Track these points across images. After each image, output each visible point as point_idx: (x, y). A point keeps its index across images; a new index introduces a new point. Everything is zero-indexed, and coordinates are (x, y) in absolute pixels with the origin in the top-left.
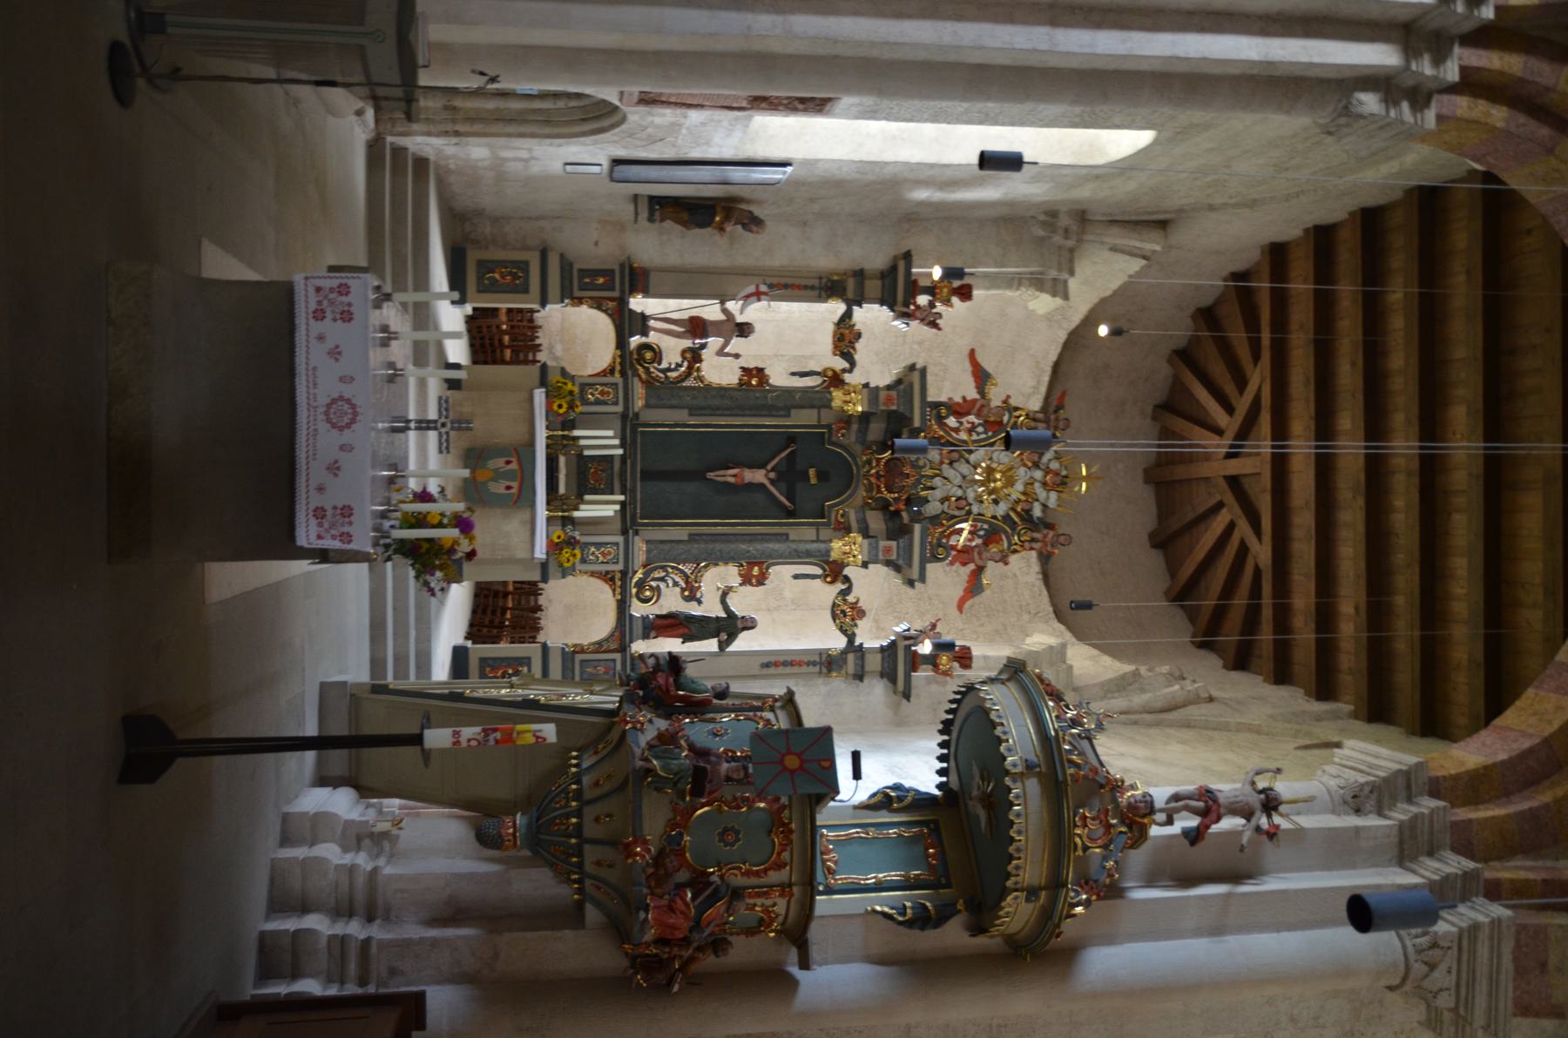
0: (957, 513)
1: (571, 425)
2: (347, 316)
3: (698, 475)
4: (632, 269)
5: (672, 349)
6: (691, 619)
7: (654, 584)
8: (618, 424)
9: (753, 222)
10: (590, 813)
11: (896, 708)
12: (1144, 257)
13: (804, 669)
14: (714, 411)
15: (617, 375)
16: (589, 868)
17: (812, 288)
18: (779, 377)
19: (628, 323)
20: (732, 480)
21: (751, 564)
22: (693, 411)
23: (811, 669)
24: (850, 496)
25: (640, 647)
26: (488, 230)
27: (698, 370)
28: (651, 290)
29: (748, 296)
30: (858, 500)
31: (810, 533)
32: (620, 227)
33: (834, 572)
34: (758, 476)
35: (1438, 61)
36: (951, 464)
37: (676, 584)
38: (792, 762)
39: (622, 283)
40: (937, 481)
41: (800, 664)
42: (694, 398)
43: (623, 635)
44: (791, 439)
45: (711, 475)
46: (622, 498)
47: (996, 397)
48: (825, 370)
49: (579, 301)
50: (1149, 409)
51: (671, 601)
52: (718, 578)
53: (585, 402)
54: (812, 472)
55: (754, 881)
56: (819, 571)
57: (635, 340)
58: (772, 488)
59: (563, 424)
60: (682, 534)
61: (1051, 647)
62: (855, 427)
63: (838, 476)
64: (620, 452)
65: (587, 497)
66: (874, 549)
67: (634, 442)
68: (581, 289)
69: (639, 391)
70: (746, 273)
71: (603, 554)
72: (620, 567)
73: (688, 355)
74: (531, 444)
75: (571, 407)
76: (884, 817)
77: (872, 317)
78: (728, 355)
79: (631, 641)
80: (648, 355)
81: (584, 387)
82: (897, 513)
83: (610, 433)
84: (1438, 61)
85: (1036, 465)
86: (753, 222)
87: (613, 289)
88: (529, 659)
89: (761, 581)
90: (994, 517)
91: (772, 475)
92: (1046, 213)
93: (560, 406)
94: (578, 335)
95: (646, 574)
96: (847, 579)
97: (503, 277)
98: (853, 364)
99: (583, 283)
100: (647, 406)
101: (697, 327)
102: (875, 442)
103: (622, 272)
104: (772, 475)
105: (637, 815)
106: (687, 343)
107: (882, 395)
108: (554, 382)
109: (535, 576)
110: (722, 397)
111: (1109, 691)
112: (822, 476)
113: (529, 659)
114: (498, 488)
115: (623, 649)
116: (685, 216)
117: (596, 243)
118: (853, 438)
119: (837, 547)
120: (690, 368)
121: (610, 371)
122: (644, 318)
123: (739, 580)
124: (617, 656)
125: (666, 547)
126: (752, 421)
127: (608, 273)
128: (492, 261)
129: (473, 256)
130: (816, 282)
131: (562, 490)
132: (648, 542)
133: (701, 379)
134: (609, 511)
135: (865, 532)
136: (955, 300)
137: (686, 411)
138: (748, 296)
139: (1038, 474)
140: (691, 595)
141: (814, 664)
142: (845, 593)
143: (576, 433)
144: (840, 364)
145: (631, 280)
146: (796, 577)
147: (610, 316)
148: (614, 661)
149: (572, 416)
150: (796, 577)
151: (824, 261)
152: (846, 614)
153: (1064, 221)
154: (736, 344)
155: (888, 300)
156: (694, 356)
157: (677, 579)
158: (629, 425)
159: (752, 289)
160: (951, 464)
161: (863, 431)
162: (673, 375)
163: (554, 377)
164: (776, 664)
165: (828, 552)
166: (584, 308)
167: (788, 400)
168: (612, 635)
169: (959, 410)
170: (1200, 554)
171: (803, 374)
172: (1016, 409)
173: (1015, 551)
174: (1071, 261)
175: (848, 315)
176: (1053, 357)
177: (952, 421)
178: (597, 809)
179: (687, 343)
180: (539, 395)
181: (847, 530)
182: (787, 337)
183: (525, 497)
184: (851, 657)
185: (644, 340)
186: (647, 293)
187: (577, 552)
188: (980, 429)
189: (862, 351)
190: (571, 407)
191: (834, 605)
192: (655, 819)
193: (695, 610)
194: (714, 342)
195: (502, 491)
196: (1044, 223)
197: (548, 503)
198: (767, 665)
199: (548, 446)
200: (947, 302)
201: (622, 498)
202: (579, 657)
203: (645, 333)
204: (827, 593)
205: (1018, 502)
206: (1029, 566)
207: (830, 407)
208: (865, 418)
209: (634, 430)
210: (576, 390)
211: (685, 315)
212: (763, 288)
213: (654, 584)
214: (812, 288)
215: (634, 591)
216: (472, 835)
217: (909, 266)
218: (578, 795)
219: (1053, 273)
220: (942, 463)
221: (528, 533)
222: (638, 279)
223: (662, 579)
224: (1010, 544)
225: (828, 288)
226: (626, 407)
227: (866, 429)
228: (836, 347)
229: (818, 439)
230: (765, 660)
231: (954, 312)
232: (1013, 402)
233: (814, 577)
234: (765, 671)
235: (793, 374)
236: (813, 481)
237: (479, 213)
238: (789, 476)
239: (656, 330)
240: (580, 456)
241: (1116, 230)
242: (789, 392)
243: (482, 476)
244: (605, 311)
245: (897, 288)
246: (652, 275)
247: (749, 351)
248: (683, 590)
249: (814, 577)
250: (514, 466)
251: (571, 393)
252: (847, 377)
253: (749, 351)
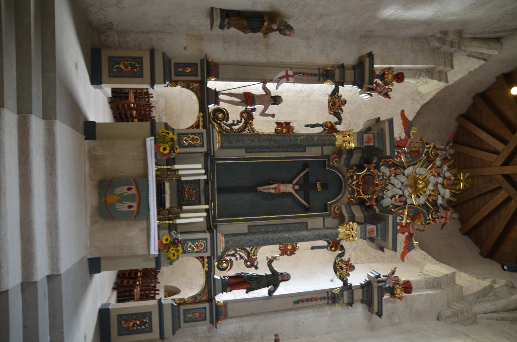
0: (399, 204)
1: (171, 161)
3: (252, 189)
4: (208, 61)
5: (235, 113)
6: (252, 278)
7: (228, 258)
8: (202, 159)
9: (286, 29)
11: (370, 320)
12: (485, 60)
13: (319, 302)
14: (261, 149)
15: (201, 127)
17: (315, 75)
18: (299, 129)
19: (206, 97)
20: (273, 191)
22: (248, 150)
23: (323, 302)
25: (221, 298)
26: (116, 40)
27: (251, 124)
28: (220, 77)
29: (281, 78)
30: (345, 199)
32: (200, 38)
33: (334, 244)
34: (288, 188)
36: (396, 175)
39: (202, 71)
41: (316, 299)
42: (252, 141)
43: (210, 291)
44: (306, 165)
45: (260, 189)
46: (207, 207)
48: (326, 123)
49: (175, 83)
51: (238, 268)
53: (182, 146)
54: (318, 184)
56: (325, 243)
57: (211, 107)
59: (167, 161)
61: (447, 275)
62: (344, 156)
64: (205, 177)
65: (185, 208)
67: (213, 170)
69: (217, 138)
70: (278, 66)
71: (197, 246)
74: (146, 176)
75: (172, 149)
77: (348, 91)
78: (268, 115)
79: (215, 295)
80: (220, 115)
81: (181, 135)
82: (370, 207)
83: (200, 166)
85: (439, 175)
86: (286, 29)
87: (197, 75)
88: (150, 313)
89: (292, 252)
91: (297, 187)
92: (442, 32)
93: (165, 149)
94: (176, 103)
96: (342, 248)
98: (340, 119)
99: (177, 72)
100: (222, 147)
101: (248, 99)
102: (354, 165)
103: (202, 65)
104: (297, 187)
106: (243, 108)
108: (162, 134)
109: (152, 265)
110: (270, 140)
111: (478, 297)
112: (324, 186)
113: (150, 313)
114: (123, 207)
115: (211, 300)
116: (245, 23)
117: (185, 48)
118: (342, 163)
120: (246, 123)
121: (197, 126)
122: (216, 93)
124: (207, 305)
125: (238, 238)
126: (283, 155)
127: (194, 65)
130: (317, 72)
131: (168, 205)
132: (225, 235)
133: (253, 130)
134: (199, 218)
137: (244, 150)
138: (281, 78)
139: (440, 180)
140: (251, 262)
141: (324, 298)
143: (176, 167)
145: (208, 69)
146: (313, 248)
147: (195, 92)
148: (205, 308)
149: (173, 155)
151: (321, 60)
152: (342, 268)
153: (452, 37)
154: (272, 109)
155: (359, 82)
156: (248, 116)
157: (242, 254)
158: (209, 160)
159: (283, 73)
160: (395, 176)
161: (348, 159)
163: (160, 130)
164: (302, 301)
166: (179, 87)
167: (309, 140)
168: (203, 291)
170: (485, 211)
174: (452, 61)
179: (243, 108)
180: (150, 142)
182: (302, 104)
183: (142, 213)
184: (345, 293)
185: (216, 106)
186: (218, 78)
187: (180, 248)
190: (172, 149)
191: (335, 263)
193: (252, 271)
195: (126, 209)
196: (439, 39)
197: (159, 214)
198: (297, 302)
199: (157, 176)
201: (207, 207)
202: (182, 308)
203: (217, 102)
204: (330, 256)
205: (430, 195)
207: (334, 145)
209: (212, 162)
210: (175, 137)
211: (241, 91)
212: (290, 73)
213: (228, 258)
214: (315, 75)
215: (216, 263)
217: (372, 64)
219: (441, 68)
220: (390, 175)
221: (145, 237)
222: (212, 70)
223: (233, 255)
224: (426, 220)
225: (323, 75)
226: (209, 148)
227: (351, 157)
228: (330, 109)
229: (322, 163)
230: (296, 299)
234: (297, 306)
235: (307, 126)
236: (319, 189)
237: (109, 26)
238: (306, 187)
239: (223, 101)
240: (179, 181)
241: (475, 43)
243: (111, 199)
244: (192, 90)
245: (363, 74)
246: (220, 67)
247: (281, 113)
248: (246, 262)
250: (134, 191)
251: (172, 139)
252: (339, 127)
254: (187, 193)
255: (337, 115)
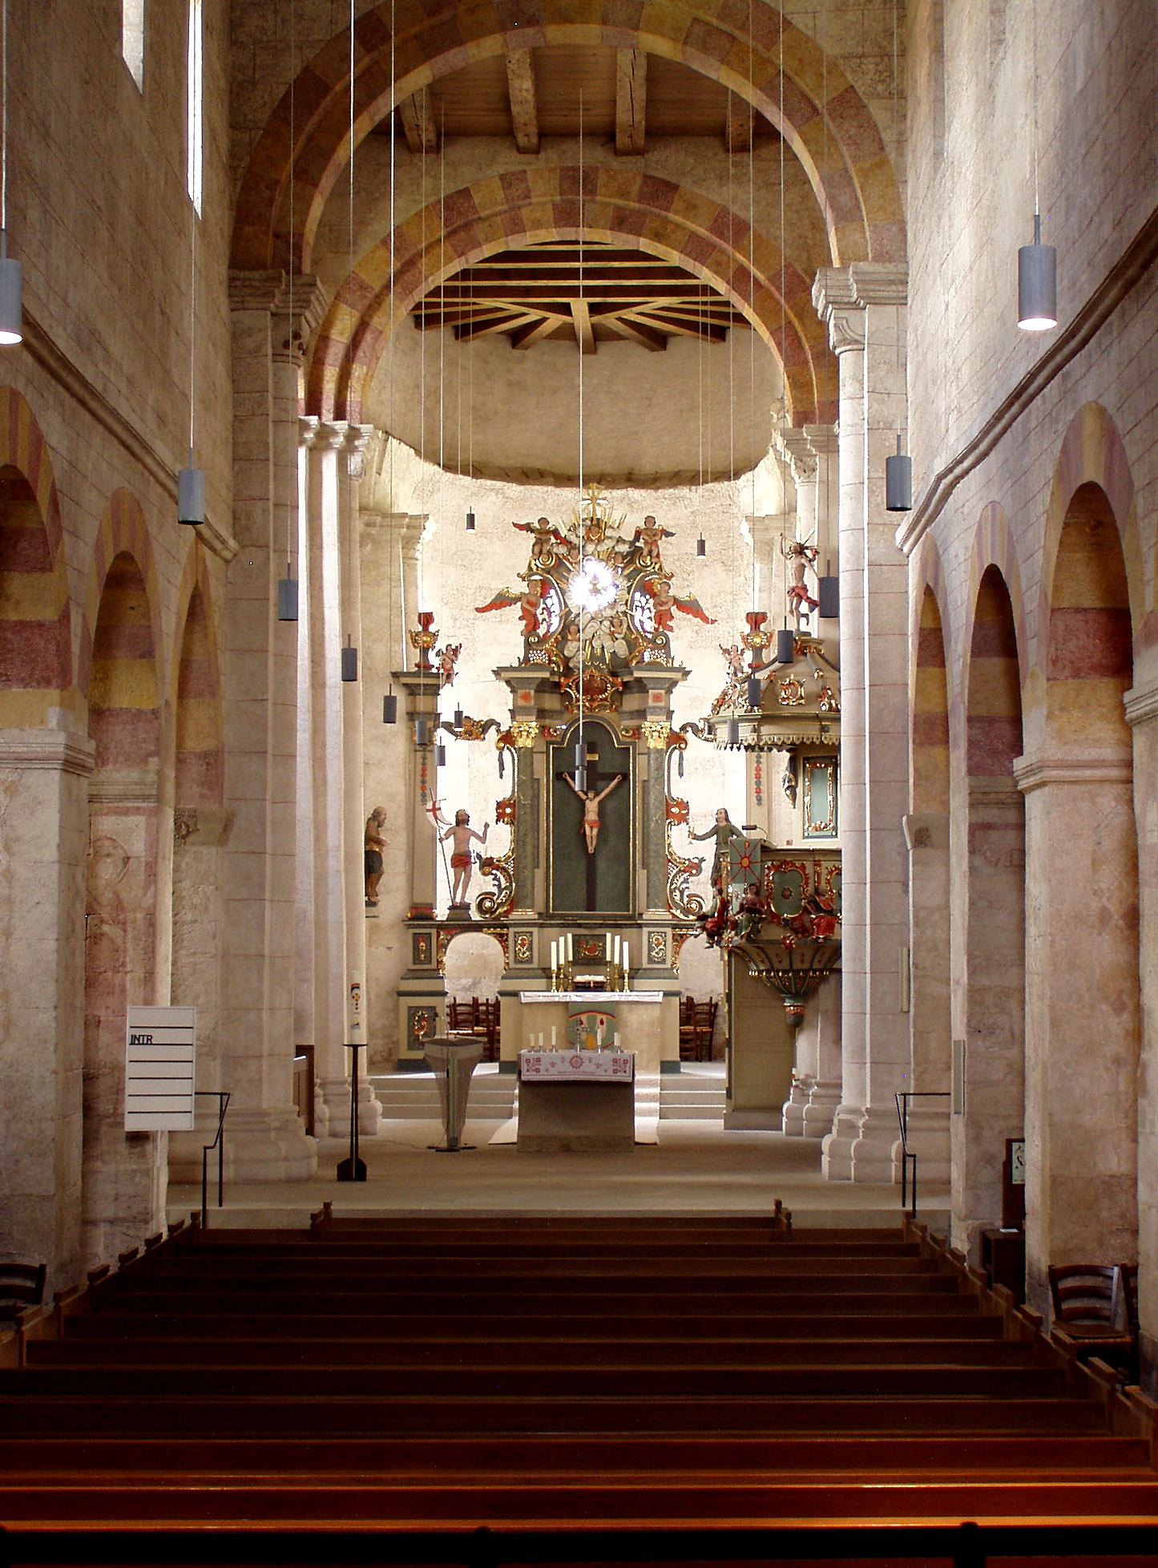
2: (538, 1060)
3: (591, 861)
5: (480, 883)
7: (686, 900)
10: (777, 966)
13: (763, 766)
16: (806, 966)
17: (424, 758)
18: (504, 788)
19: (459, 922)
20: (595, 831)
21: (669, 814)
24: (609, 724)
31: (642, 760)
33: (676, 740)
34: (592, 807)
35: (335, 433)
37: (686, 881)
38: (745, 862)
39: (424, 927)
40: (596, 644)
41: (758, 769)
45: (591, 850)
47: (520, 587)
50: (517, 353)
52: (680, 842)
55: (811, 881)
57: (475, 916)
58: (603, 795)
60: (641, 875)
63: (596, 735)
66: (656, 711)
68: (430, 962)
69: (517, 915)
72: (669, 931)
73: (487, 869)
76: (799, 790)
80: (488, 904)
82: (625, 684)
84: (335, 433)
90: (629, 588)
91: (591, 795)
95: (677, 907)
96: (683, 728)
97: (422, 1028)
100: (532, 907)
101: (461, 861)
102: (562, 702)
104: (591, 795)
105: (770, 942)
106: (475, 868)
107: (521, 703)
119: (655, 743)
121: (502, 939)
123: (683, 825)
128: (409, 1036)
129: (406, 1054)
131: (600, 978)
135: (642, 714)
136: (432, 628)
140: (694, 867)
142: (696, 731)
143: (554, 967)
144: (492, 735)
145: (422, 919)
146: (681, 775)
150: (681, 775)
154: (475, 825)
155: (434, 690)
156: (488, 864)
162: (504, 884)
164: (758, 791)
165: (658, 751)
169: (532, 625)
171: (502, 767)
172: (530, 568)
173: (661, 568)
174: (393, 516)
175: (448, 726)
176: (467, 480)
177: (542, 631)
178: (775, 960)
179: (475, 868)
181: (637, 732)
183: (610, 1011)
185: (473, 907)
186: (431, 906)
188: (548, 601)
189: (478, 715)
192: (776, 933)
193: (708, 867)
194: (475, 846)
198: (759, 800)
200: (435, 636)
203: (467, 907)
204: (696, 746)
206: (683, 498)
208: (541, 714)
209: (552, 917)
211: (451, 871)
212: (430, 806)
213: (686, 900)
216: (801, 1031)
218: (768, 972)
222: (420, 914)
223: (682, 893)
226: (534, 925)
231: (446, 632)
232: (524, 571)
233: (681, 757)
239: (463, 897)
240: (574, 963)
242: (520, 785)
244: (449, 941)
246: (417, 900)
247: (482, 815)
248: (691, 875)
249: (681, 757)
250: (584, 1018)
252: (504, 728)
253: (482, 815)
254: (588, 956)
255: (485, 727)
